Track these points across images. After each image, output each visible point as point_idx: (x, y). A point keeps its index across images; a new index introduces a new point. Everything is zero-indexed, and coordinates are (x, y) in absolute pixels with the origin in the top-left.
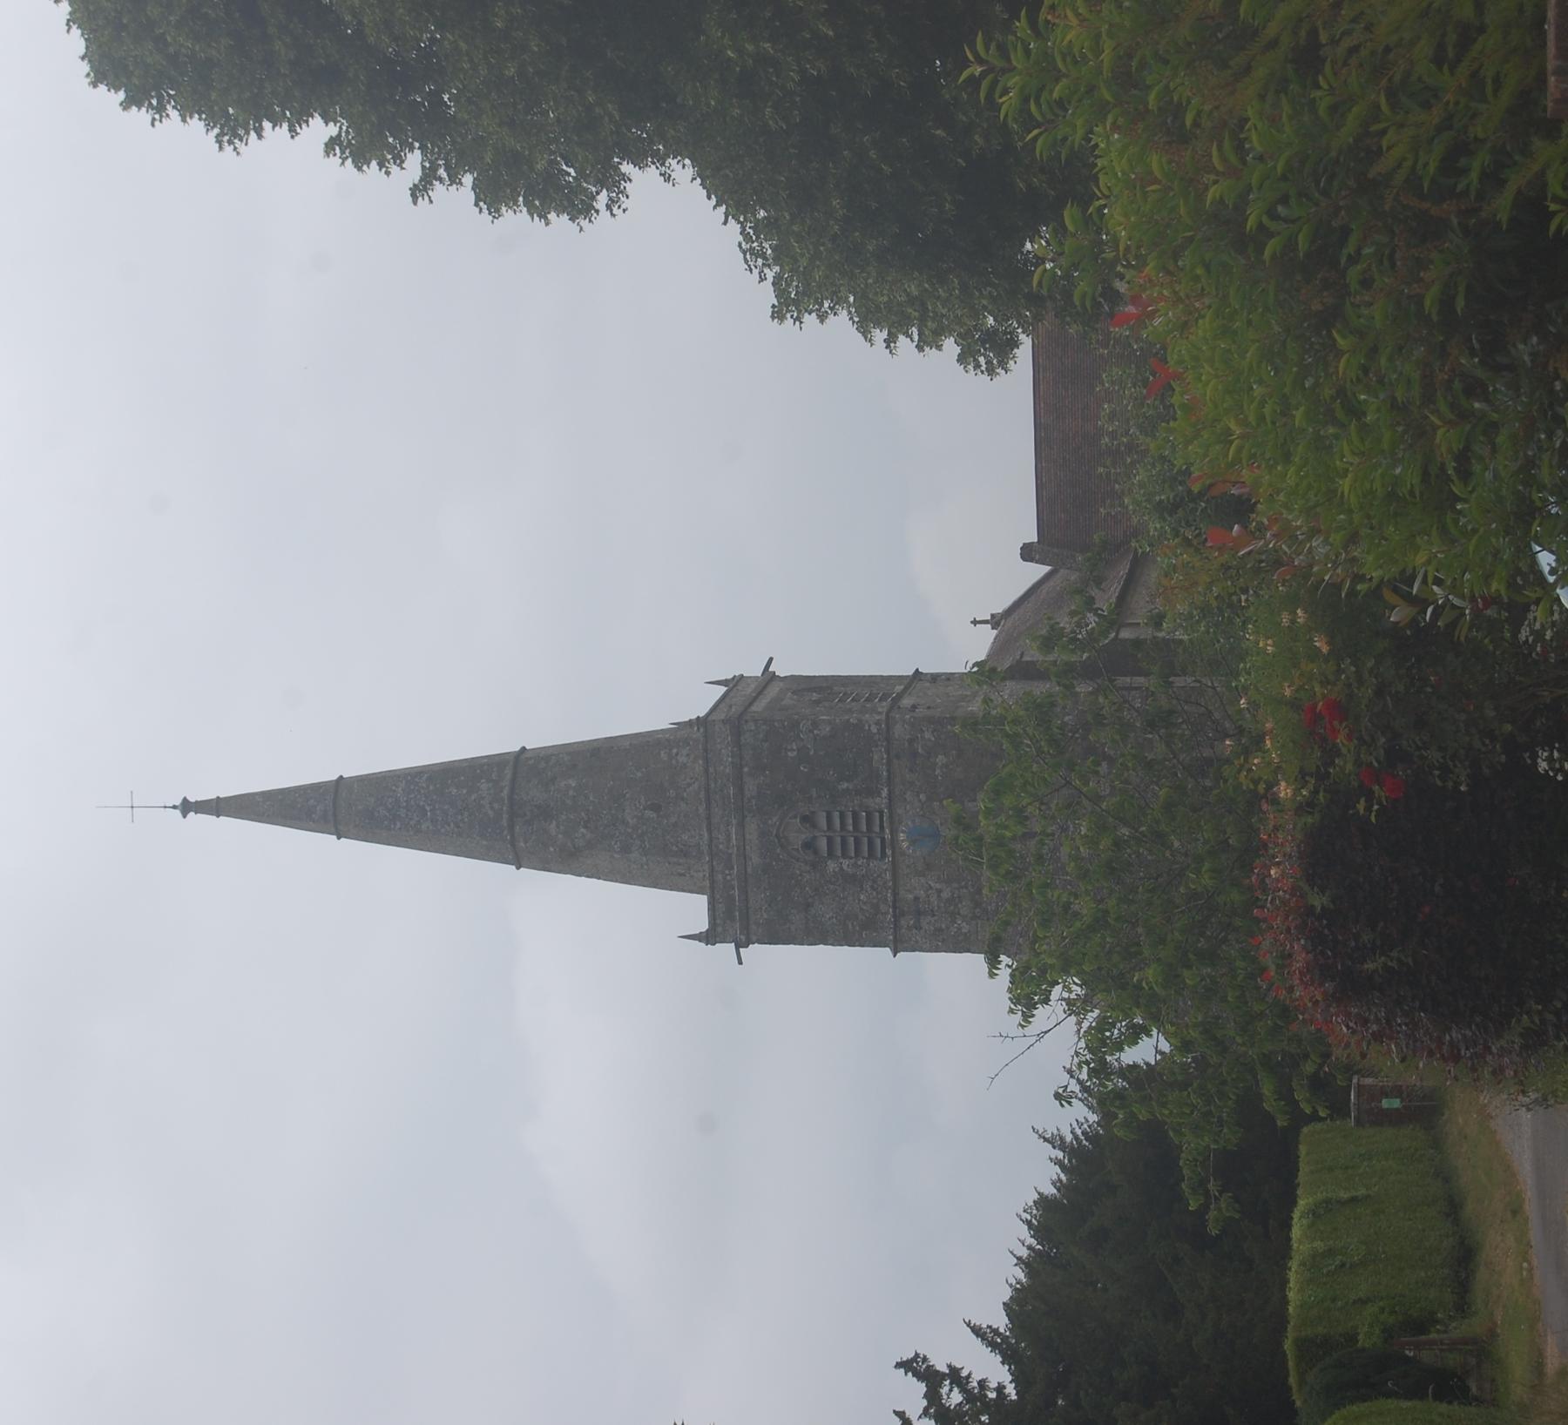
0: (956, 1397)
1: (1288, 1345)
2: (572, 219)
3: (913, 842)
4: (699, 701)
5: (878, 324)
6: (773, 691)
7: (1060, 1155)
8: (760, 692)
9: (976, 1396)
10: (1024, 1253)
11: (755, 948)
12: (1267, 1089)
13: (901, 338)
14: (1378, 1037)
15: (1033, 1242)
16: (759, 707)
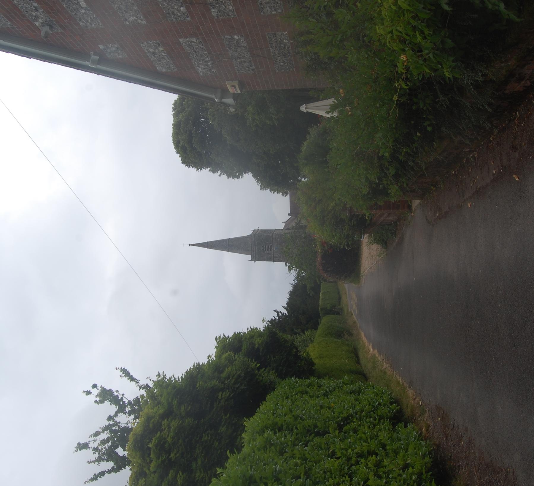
0: (281, 315)
1: (319, 309)
2: (237, 179)
3: (275, 249)
4: (250, 233)
5: (272, 191)
6: (259, 231)
7: (292, 286)
8: (257, 232)
9: (283, 314)
10: (288, 297)
11: (257, 262)
12: (317, 280)
13: (275, 192)
14: (329, 276)
15: (289, 296)
16: (257, 233)
